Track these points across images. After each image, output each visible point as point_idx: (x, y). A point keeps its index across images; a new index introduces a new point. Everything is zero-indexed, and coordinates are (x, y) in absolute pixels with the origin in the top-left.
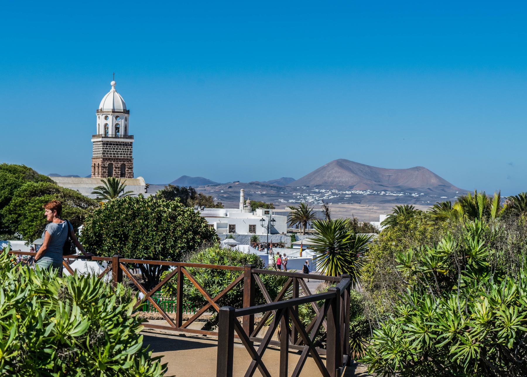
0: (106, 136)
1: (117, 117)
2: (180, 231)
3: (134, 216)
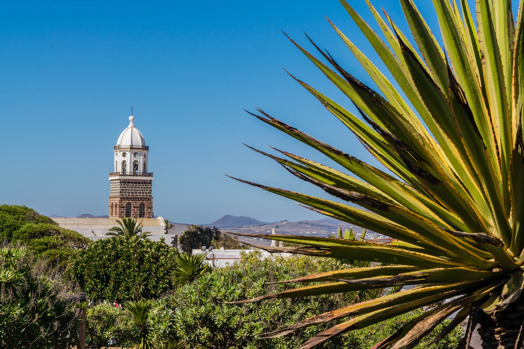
0: (124, 173)
1: (135, 154)
2: (162, 271)
3: (117, 257)
